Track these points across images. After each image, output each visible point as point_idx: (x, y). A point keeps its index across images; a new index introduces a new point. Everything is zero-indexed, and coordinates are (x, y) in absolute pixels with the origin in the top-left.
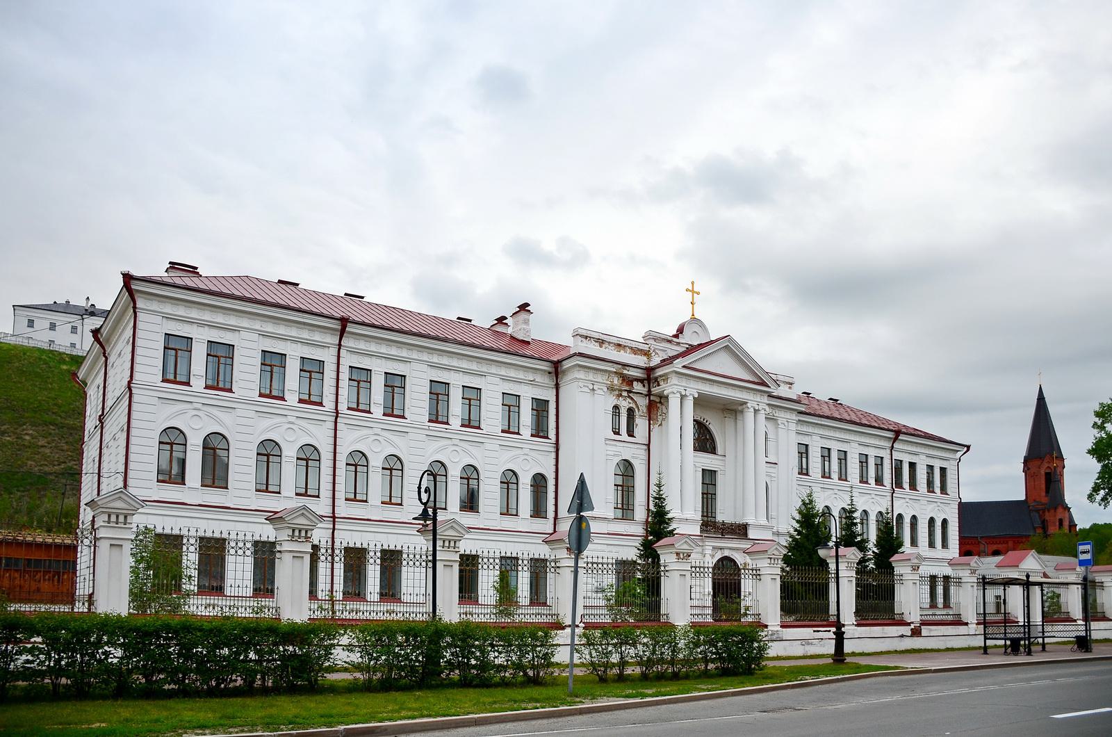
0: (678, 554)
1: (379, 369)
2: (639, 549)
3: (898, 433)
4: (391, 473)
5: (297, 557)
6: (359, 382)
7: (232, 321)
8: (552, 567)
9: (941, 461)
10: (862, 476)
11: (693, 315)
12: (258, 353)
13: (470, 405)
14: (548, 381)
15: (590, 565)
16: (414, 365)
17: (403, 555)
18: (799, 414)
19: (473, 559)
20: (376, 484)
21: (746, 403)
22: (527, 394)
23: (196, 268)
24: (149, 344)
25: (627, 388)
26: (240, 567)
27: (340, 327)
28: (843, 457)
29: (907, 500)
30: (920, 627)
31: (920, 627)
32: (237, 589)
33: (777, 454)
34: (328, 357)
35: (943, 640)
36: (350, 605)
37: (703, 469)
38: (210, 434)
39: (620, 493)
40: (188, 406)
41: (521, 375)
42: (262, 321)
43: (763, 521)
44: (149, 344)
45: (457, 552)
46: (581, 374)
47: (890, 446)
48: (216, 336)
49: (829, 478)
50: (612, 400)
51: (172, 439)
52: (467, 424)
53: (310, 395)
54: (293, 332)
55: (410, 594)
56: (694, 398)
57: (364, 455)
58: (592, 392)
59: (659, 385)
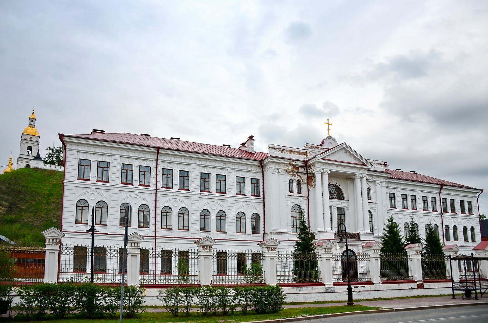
0: (268, 248)
1: (176, 169)
2: (295, 247)
3: (442, 185)
4: (183, 216)
5: (52, 252)
6: (167, 175)
7: (108, 151)
8: (367, 258)
9: (432, 194)
10: (425, 207)
11: (329, 135)
12: (77, 160)
13: (221, 183)
14: (259, 170)
15: (280, 256)
16: (193, 166)
17: (173, 253)
18: (387, 179)
19: (244, 255)
20: (176, 220)
21: (356, 174)
22: (248, 177)
23: (104, 131)
24: (72, 164)
25: (296, 171)
26: (112, 260)
27: (157, 151)
28: (414, 199)
30: (423, 283)
31: (423, 283)
32: (288, 272)
33: (376, 198)
34: (152, 165)
35: (437, 291)
36: (163, 277)
37: (337, 207)
38: (204, 210)
39: (295, 220)
40: (89, 190)
41: (245, 168)
42: (121, 151)
43: (368, 231)
44: (72, 164)
45: (138, 249)
46: (272, 166)
47: (439, 192)
48: (101, 158)
49: (407, 209)
50: (289, 177)
52: (220, 191)
53: (144, 182)
54: (136, 155)
55: (196, 272)
56: (328, 173)
57: (244, 213)
58: (278, 174)
59: (311, 168)
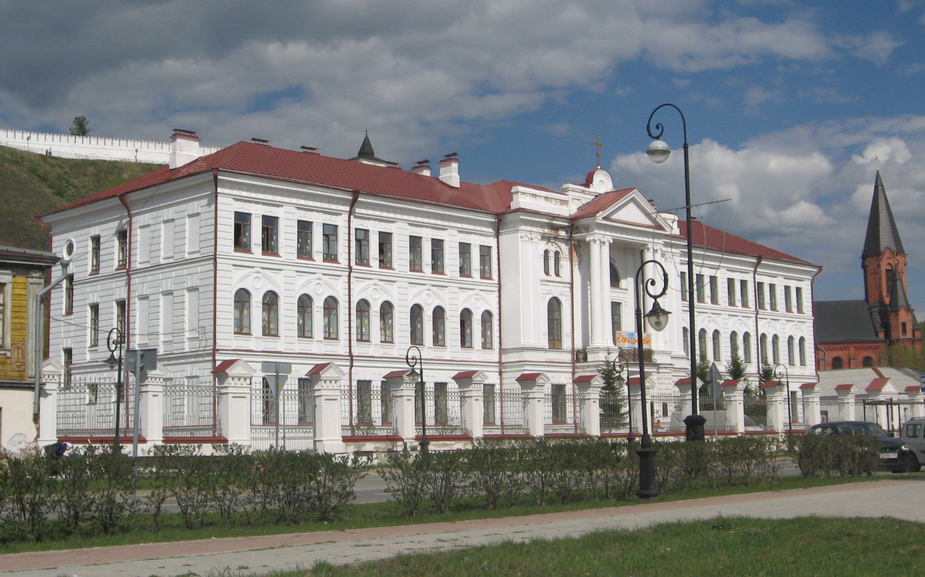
21: (647, 245)
29: (769, 320)
50: (543, 246)
51: (242, 298)
56: (610, 243)
